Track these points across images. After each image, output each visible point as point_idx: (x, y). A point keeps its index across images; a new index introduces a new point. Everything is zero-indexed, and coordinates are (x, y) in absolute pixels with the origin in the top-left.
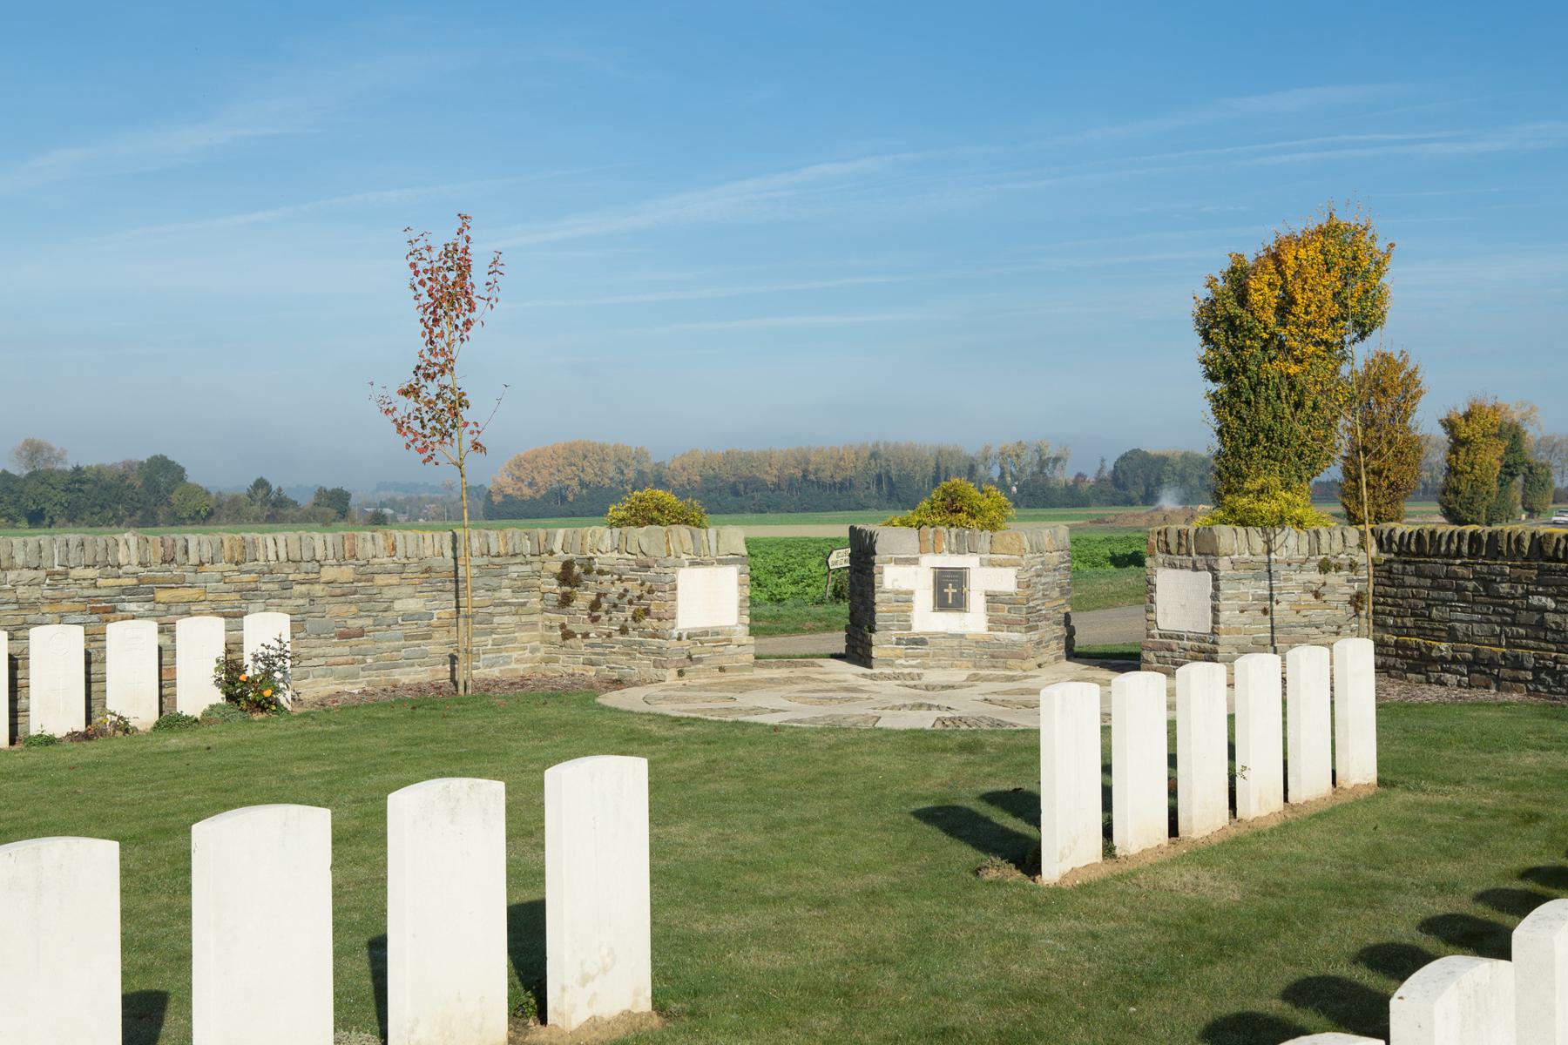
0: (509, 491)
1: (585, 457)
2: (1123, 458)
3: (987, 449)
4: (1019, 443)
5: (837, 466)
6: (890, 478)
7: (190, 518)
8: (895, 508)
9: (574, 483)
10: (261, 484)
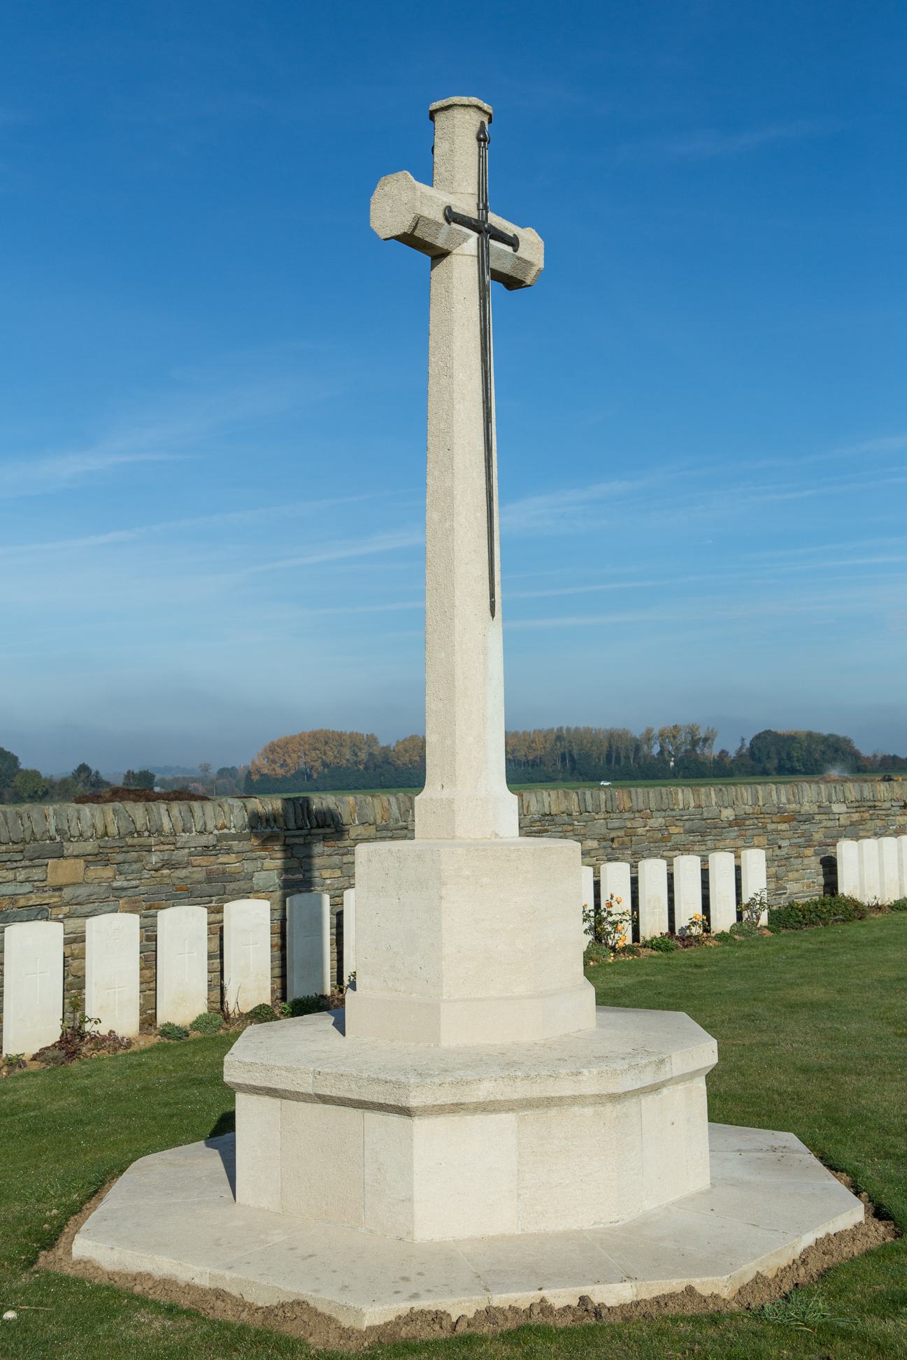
0: (265, 771)
1: (326, 743)
2: (758, 737)
3: (649, 731)
4: (675, 727)
5: (530, 747)
6: (571, 756)
7: (30, 797)
8: (578, 780)
9: (318, 764)
10: (83, 768)
